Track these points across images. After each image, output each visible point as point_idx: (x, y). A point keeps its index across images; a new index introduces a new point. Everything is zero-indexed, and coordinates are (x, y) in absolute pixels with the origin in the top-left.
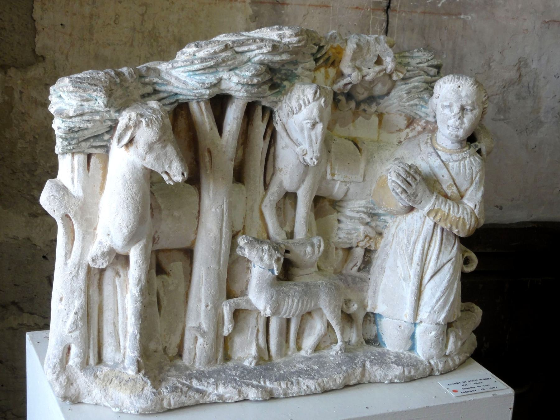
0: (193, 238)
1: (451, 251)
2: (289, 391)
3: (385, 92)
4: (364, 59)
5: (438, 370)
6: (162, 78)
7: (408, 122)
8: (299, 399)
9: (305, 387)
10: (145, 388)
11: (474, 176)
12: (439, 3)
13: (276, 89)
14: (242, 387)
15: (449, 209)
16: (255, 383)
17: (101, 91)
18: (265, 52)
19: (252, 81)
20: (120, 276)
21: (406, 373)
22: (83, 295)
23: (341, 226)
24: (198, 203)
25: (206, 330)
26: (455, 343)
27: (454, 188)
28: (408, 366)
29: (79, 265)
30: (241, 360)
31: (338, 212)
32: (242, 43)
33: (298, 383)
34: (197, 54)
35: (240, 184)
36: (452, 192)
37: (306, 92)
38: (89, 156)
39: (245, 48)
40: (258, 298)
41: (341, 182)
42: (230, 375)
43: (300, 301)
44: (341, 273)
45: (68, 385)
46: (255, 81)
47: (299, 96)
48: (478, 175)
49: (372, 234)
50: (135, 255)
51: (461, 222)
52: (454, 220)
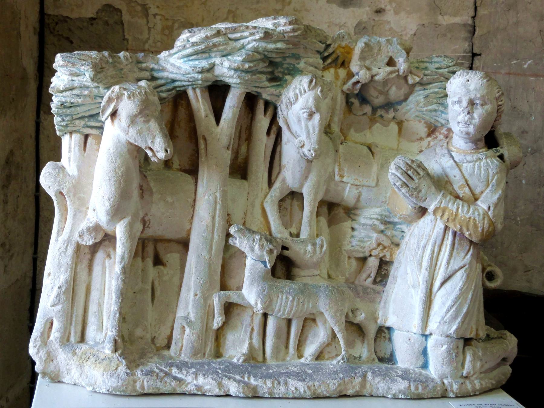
0: (188, 228)
1: (464, 258)
2: (276, 391)
3: (402, 98)
4: (375, 60)
5: (453, 391)
6: (160, 65)
7: (429, 129)
8: (285, 401)
9: (293, 389)
10: (119, 368)
11: (490, 178)
12: (525, 64)
13: (278, 82)
14: (222, 379)
15: (458, 209)
16: (238, 377)
17: (88, 65)
18: (257, 38)
19: (243, 66)
20: (110, 258)
21: (413, 388)
22: (69, 270)
23: (355, 233)
24: (194, 191)
25: (193, 320)
26: (473, 361)
27: (467, 189)
28: (415, 381)
29: (68, 242)
30: (232, 357)
31: (353, 220)
32: (234, 30)
33: (286, 383)
34: (190, 39)
35: (243, 181)
36: (464, 193)
37: (302, 82)
38: (86, 137)
39: (238, 35)
40: (250, 293)
41: (352, 185)
42: (214, 368)
43: (296, 299)
44: (353, 283)
45: (48, 360)
46: (247, 66)
47: (296, 86)
48: (496, 178)
49: (387, 243)
50: (120, 231)
51: (471, 222)
52: (464, 220)
